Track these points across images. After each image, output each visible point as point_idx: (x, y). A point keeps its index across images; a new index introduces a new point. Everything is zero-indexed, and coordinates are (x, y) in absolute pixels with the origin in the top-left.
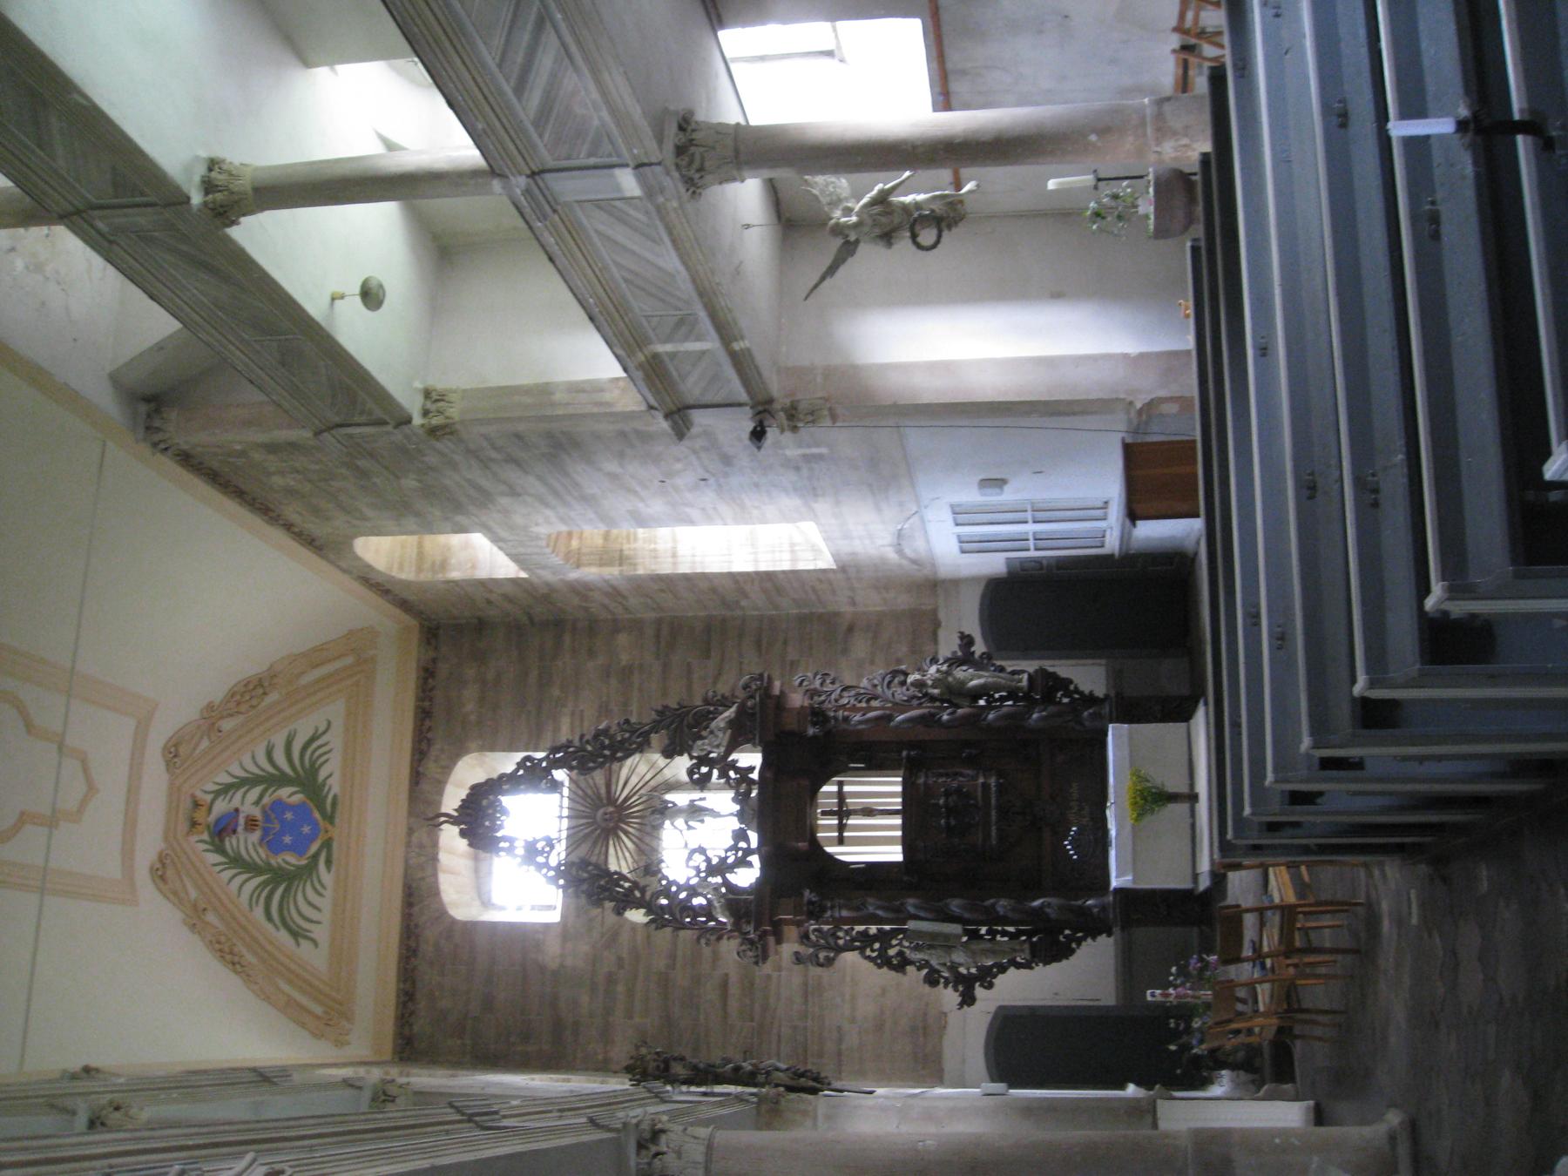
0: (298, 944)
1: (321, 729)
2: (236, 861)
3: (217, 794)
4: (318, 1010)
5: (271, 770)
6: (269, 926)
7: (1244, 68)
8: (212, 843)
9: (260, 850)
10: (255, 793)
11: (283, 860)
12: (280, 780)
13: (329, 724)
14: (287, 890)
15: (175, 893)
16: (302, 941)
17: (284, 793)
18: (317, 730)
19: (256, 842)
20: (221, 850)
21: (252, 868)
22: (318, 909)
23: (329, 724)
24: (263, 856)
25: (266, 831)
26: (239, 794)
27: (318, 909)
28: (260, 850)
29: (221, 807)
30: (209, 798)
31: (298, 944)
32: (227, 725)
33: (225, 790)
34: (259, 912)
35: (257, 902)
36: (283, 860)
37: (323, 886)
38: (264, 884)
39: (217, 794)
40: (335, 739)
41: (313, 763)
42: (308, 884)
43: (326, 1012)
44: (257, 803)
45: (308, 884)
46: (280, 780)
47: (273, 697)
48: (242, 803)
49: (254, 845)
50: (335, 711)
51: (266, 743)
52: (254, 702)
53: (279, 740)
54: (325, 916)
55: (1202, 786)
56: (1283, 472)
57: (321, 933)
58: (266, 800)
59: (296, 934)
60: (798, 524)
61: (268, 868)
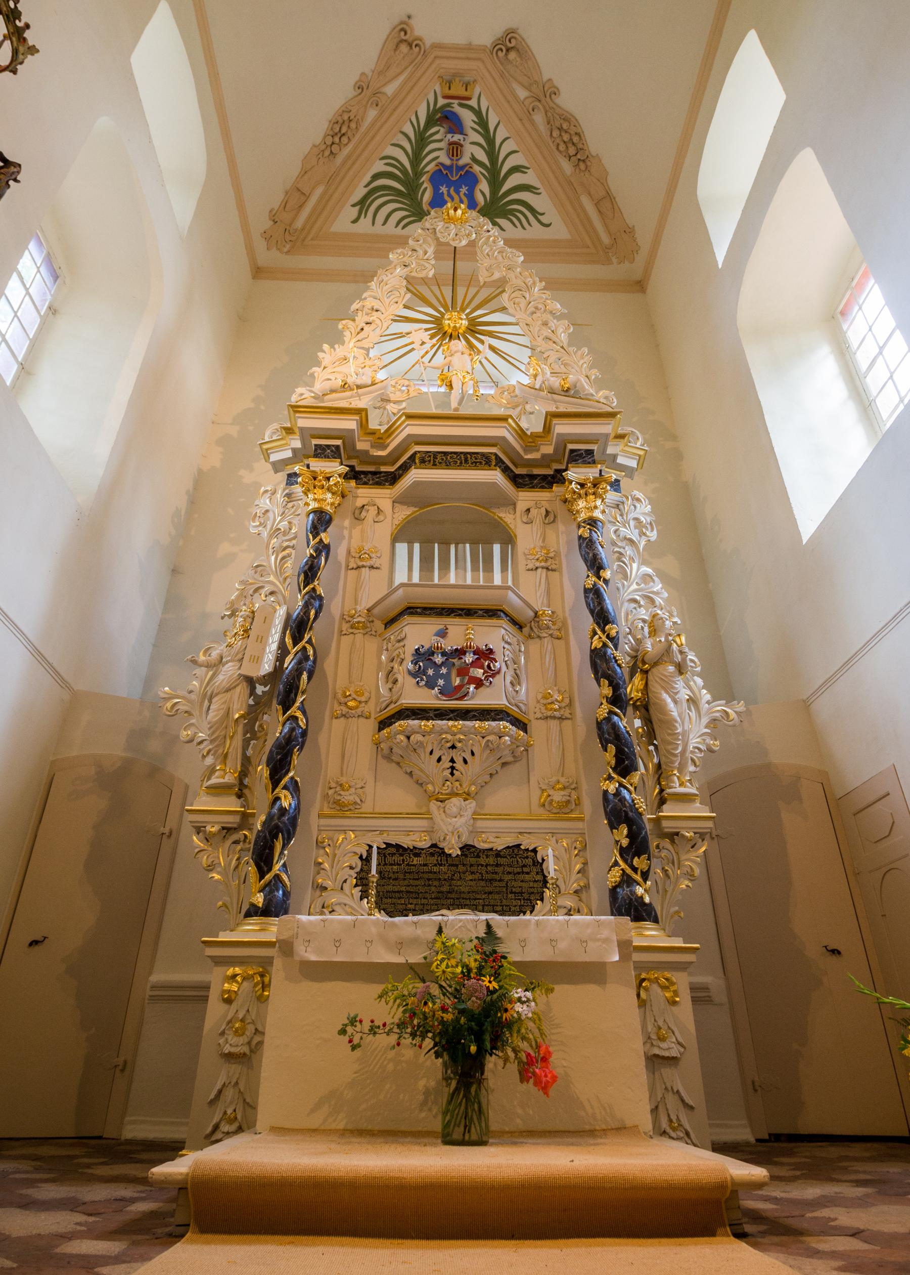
0: (353, 206)
1: (542, 218)
2: (421, 141)
3: (478, 113)
4: (299, 224)
5: (505, 188)
6: (368, 178)
7: (264, 847)
8: (436, 111)
9: (432, 165)
10: (482, 156)
11: (426, 189)
12: (495, 182)
13: (548, 225)
14: (399, 193)
15: (388, 67)
16: (358, 208)
17: (484, 186)
18: (543, 214)
19: (441, 160)
20: (430, 122)
21: (416, 158)
22: (384, 224)
23: (548, 225)
24: (427, 169)
25: (449, 168)
26: (481, 141)
27: (384, 224)
28: (432, 165)
29: (468, 118)
30: (473, 103)
31: (353, 206)
32: (539, 118)
33: (483, 123)
34: (380, 166)
35: (386, 164)
36: (426, 189)
37: (403, 228)
38: (404, 171)
39: (478, 113)
40: (535, 231)
41: (512, 212)
42: (405, 213)
43: (296, 230)
44: (474, 159)
45: (405, 213)
46: (495, 182)
47: (567, 167)
48: (473, 143)
49: (437, 158)
50: (560, 230)
51: (527, 165)
52: (562, 147)
53: (529, 178)
54: (379, 229)
55: (724, 1211)
56: (483, 562)
57: (365, 225)
58: (477, 169)
59: (363, 204)
60: (887, 311)
61: (418, 174)
